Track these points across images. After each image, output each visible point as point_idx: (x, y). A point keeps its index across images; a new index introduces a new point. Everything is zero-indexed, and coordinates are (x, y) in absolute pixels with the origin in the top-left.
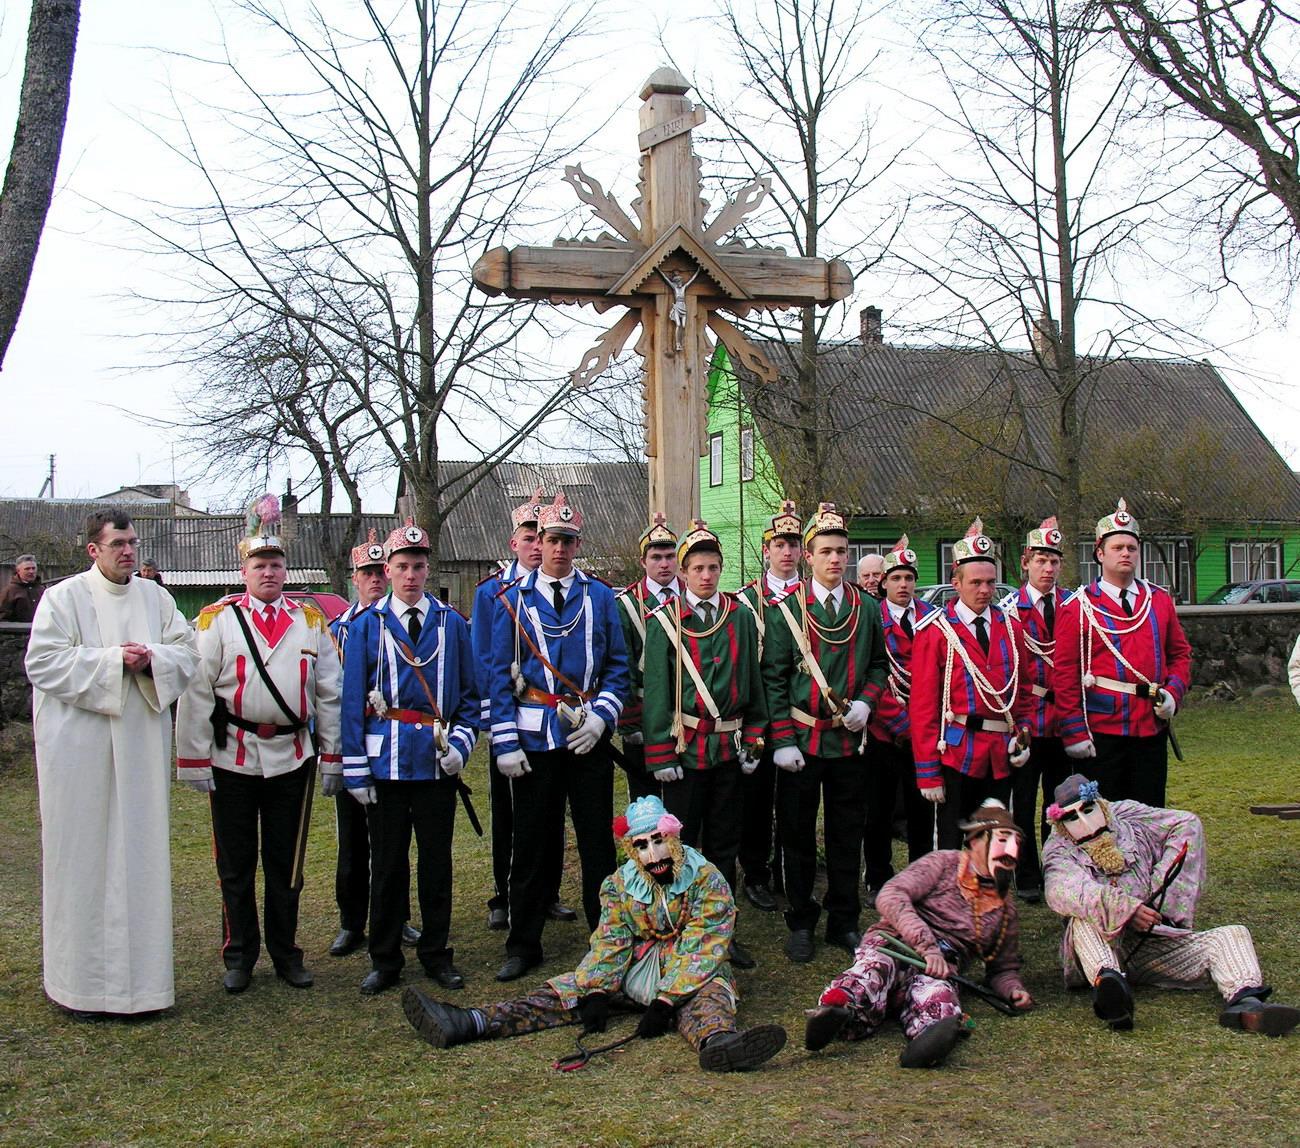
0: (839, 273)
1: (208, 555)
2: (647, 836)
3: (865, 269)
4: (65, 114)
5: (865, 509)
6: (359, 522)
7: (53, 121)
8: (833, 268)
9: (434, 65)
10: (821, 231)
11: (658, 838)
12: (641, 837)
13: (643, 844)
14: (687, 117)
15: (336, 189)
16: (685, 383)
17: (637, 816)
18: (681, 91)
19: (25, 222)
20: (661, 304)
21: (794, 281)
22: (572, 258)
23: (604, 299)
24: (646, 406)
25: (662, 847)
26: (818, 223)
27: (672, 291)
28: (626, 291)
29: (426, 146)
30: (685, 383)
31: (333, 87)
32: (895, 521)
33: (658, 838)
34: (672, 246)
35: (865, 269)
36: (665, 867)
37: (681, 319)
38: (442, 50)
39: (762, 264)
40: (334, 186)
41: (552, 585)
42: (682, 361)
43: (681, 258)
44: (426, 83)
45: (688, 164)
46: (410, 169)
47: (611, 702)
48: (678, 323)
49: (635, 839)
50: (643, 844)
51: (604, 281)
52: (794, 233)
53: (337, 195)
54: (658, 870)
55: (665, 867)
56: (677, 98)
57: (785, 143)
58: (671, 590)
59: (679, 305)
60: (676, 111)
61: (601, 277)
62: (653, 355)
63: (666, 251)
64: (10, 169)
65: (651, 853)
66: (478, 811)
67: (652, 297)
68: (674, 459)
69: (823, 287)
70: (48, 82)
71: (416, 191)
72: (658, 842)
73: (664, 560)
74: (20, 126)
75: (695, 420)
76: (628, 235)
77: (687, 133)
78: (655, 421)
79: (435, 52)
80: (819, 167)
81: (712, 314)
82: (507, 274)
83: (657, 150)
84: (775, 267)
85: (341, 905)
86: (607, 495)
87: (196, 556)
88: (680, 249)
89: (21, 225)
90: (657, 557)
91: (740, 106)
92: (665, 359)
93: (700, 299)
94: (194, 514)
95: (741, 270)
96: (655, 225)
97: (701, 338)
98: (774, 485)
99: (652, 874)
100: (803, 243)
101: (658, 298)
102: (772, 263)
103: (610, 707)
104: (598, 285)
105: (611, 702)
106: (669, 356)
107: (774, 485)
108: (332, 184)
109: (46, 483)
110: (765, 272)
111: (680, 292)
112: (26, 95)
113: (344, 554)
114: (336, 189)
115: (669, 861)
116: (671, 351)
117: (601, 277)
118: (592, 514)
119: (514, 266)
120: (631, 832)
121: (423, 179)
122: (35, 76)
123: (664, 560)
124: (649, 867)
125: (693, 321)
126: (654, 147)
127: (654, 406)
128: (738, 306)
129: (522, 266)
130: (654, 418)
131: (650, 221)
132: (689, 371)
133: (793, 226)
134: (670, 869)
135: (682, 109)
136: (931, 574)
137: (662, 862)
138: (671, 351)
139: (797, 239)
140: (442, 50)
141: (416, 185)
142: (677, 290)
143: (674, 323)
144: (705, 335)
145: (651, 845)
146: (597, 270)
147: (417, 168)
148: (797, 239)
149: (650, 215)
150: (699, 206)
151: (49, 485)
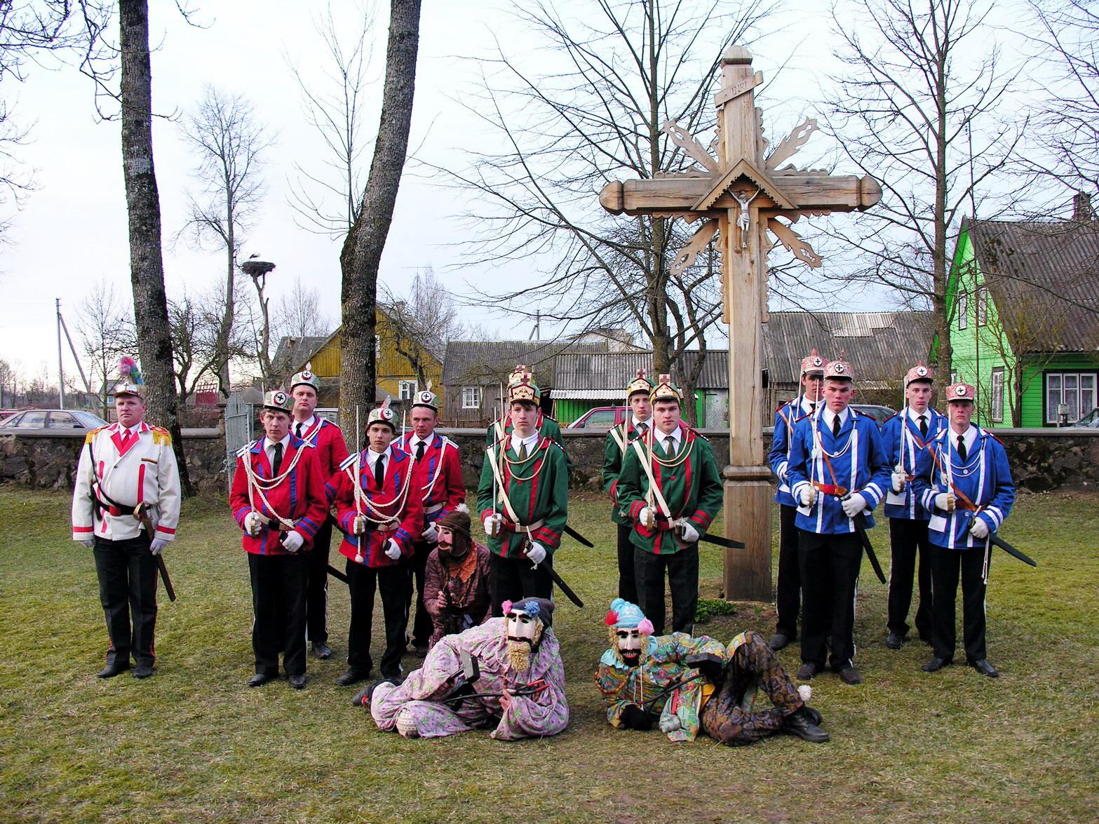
0: (867, 186)
1: (613, 379)
2: (629, 630)
3: (989, 172)
4: (412, 102)
5: (1066, 346)
6: (704, 357)
7: (403, 107)
8: (863, 182)
9: (660, 46)
10: (948, 147)
11: (636, 634)
12: (625, 630)
13: (624, 635)
14: (749, 80)
15: (587, 138)
16: (749, 270)
17: (625, 614)
18: (748, 62)
19: (387, 173)
20: (731, 215)
21: (832, 193)
22: (666, 186)
23: (690, 213)
24: (723, 288)
25: (636, 640)
26: (947, 140)
27: (739, 206)
28: (703, 207)
29: (655, 104)
30: (749, 270)
31: (593, 68)
32: (1088, 356)
33: (636, 634)
34: (737, 173)
35: (989, 172)
36: (635, 654)
37: (745, 225)
38: (665, 36)
39: (808, 183)
40: (585, 136)
41: (811, 405)
42: (748, 255)
43: (743, 180)
44: (654, 61)
45: (751, 114)
46: (645, 120)
47: (875, 491)
48: (743, 228)
49: (620, 629)
50: (624, 635)
51: (690, 201)
52: (927, 149)
53: (587, 142)
54: (629, 655)
55: (635, 654)
56: (747, 66)
57: (917, 83)
58: (673, 438)
59: (744, 216)
60: (742, 76)
61: (687, 198)
62: (727, 252)
63: (732, 177)
64: (379, 139)
65: (628, 643)
66: (880, 558)
67: (725, 210)
68: (741, 325)
69: (855, 196)
70: (398, 82)
71: (648, 135)
72: (635, 637)
73: (667, 411)
74: (384, 112)
75: (756, 297)
76: (710, 167)
77: (751, 91)
78: (728, 299)
79: (660, 37)
80: (948, 97)
81: (772, 221)
82: (621, 200)
83: (728, 105)
84: (818, 184)
85: (908, 611)
86: (904, 335)
87: (605, 380)
88: (743, 175)
89: (385, 175)
90: (662, 410)
91: (886, 58)
92: (735, 254)
93: (761, 210)
94: (639, 350)
95: (791, 188)
96: (727, 160)
97: (763, 238)
98: (992, 330)
99: (624, 657)
100: (935, 155)
101: (729, 211)
102: (816, 181)
103: (875, 496)
104: (685, 204)
105: (875, 491)
106: (738, 252)
107: (992, 330)
108: (584, 135)
109: (534, 329)
110: (810, 188)
111: (744, 206)
112: (386, 92)
113: (693, 379)
114: (587, 138)
115: (638, 651)
116: (739, 248)
117: (687, 198)
118: (892, 348)
119: (625, 194)
120: (617, 625)
121: (653, 126)
122: (391, 79)
123: (667, 411)
124: (623, 652)
125: (755, 226)
126: (726, 103)
127: (727, 288)
128: (792, 214)
129: (631, 193)
130: (728, 296)
131: (724, 157)
132: (752, 262)
133: (926, 143)
134: (637, 657)
135: (745, 75)
136: (1038, 407)
137: (634, 650)
138: (739, 248)
139: (930, 154)
140: (665, 36)
141: (648, 131)
142: (742, 205)
143: (740, 227)
144: (766, 237)
145: (629, 637)
146: (684, 194)
147: (649, 119)
148: (930, 154)
149: (724, 151)
150: (761, 143)
151: (536, 331)
